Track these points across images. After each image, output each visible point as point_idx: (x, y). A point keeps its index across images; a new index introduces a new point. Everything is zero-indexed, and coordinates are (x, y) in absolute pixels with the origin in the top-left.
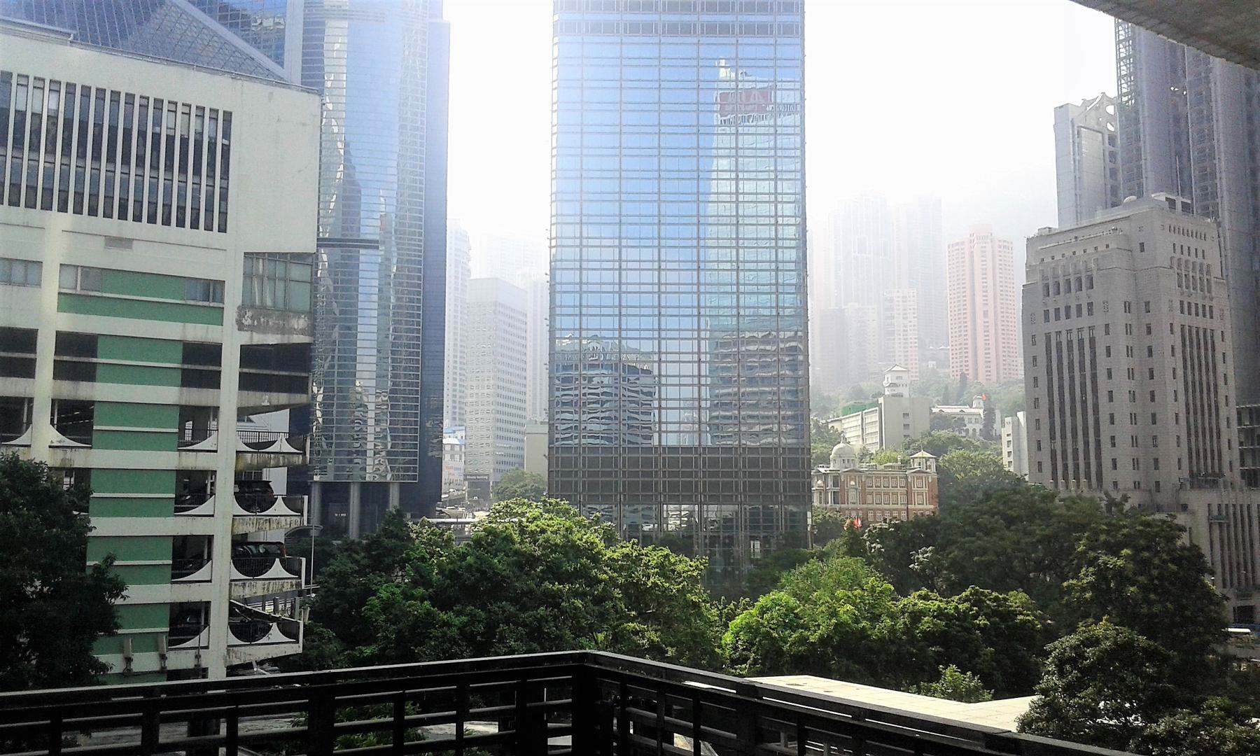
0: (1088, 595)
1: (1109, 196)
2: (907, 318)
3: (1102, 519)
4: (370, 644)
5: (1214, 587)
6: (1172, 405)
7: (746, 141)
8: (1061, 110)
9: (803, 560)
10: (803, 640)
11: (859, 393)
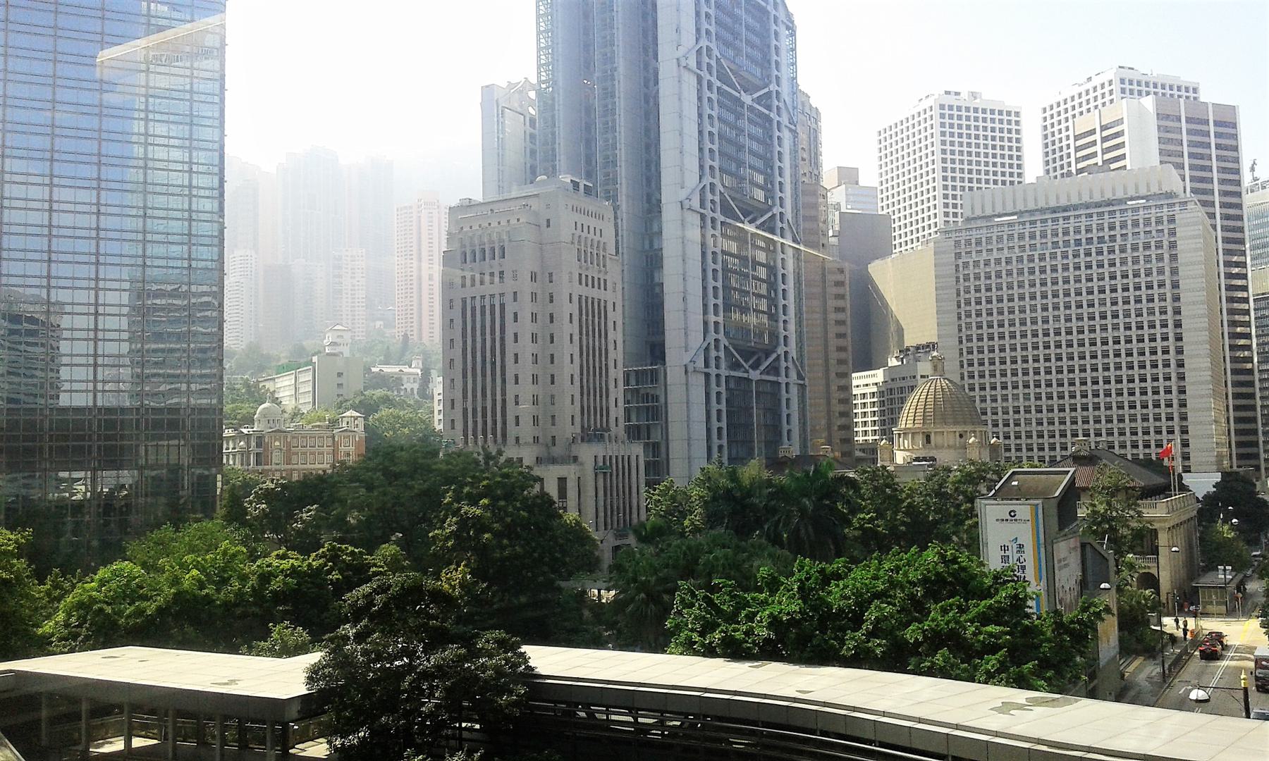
6: (568, 368)
8: (487, 90)
11: (300, 351)
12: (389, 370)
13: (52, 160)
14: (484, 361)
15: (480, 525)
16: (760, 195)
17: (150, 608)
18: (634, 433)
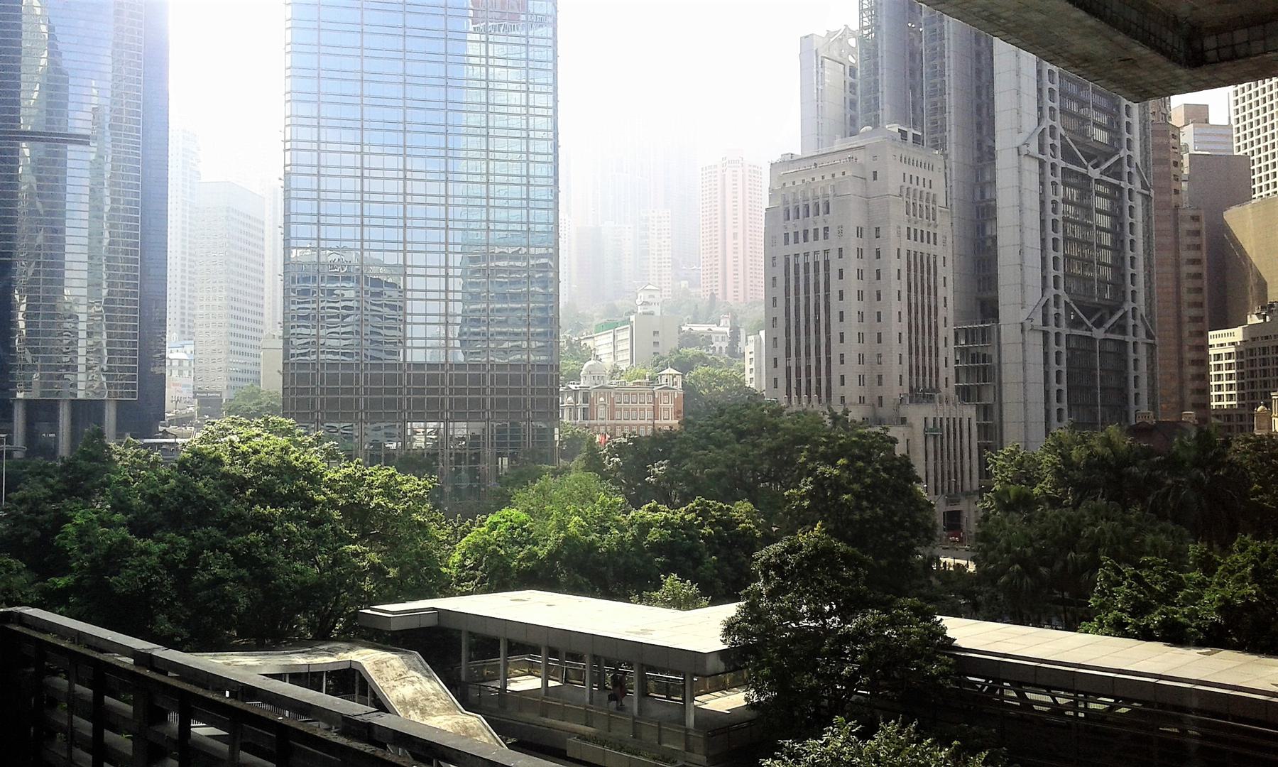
1: (848, 126)
3: (823, 432)
4: (63, 576)
5: (926, 495)
6: (896, 326)
7: (495, 50)
9: (536, 477)
10: (532, 556)
12: (698, 329)
13: (405, 131)
14: (807, 321)
15: (837, 486)
16: (1101, 136)
17: (542, 554)
18: (965, 394)
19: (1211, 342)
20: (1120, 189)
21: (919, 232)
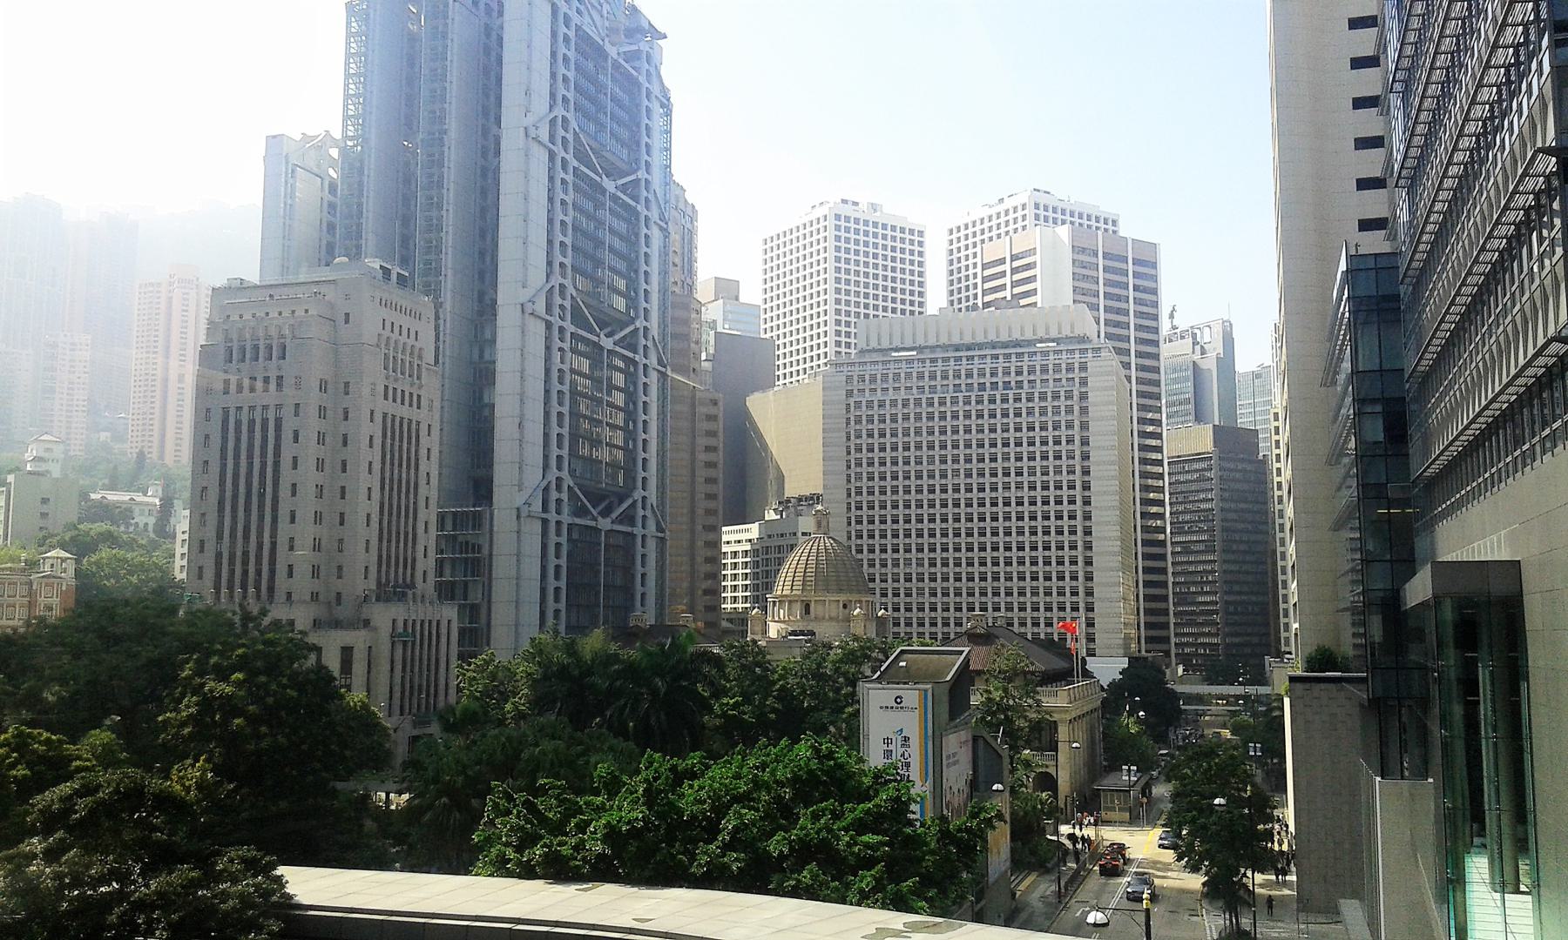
0: (186, 731)
2: (74, 372)
6: (364, 505)
8: (274, 140)
15: (230, 707)
18: (446, 592)
19: (725, 538)
20: (635, 363)
21: (399, 392)
